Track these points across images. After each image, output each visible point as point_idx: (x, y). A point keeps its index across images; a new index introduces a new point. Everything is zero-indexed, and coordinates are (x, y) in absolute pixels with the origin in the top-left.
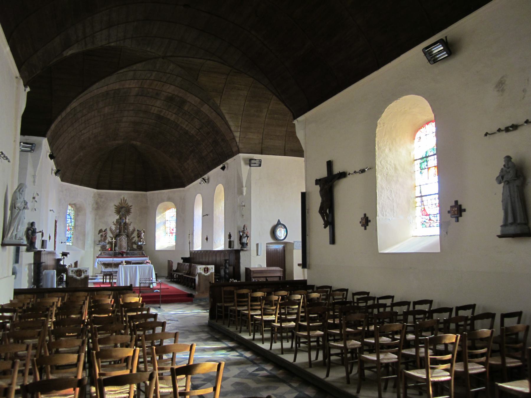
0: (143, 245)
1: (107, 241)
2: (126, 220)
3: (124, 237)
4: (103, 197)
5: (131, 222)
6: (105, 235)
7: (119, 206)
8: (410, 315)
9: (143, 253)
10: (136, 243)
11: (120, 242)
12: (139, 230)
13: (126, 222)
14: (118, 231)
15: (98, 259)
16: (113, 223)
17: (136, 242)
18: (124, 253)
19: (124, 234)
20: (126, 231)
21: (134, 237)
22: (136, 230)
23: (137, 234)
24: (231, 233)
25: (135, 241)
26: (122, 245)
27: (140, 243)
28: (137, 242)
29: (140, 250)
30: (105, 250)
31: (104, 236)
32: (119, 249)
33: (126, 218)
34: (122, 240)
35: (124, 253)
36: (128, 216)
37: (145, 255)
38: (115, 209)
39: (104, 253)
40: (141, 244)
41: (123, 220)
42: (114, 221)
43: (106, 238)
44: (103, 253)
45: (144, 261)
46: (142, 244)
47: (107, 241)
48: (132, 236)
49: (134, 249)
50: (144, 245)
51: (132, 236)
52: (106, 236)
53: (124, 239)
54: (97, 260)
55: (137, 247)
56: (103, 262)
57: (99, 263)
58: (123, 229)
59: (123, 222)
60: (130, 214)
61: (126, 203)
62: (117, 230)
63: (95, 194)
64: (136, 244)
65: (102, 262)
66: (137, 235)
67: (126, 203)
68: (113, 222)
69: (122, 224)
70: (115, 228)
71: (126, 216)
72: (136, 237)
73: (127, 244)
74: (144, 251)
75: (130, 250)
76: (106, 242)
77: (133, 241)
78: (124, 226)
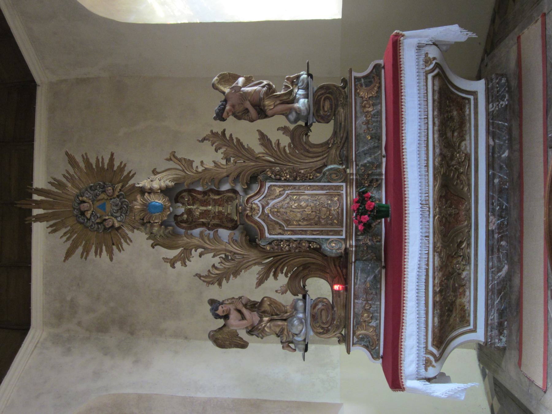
0: (315, 86)
1: (288, 299)
2: (151, 191)
3: (257, 201)
4: (69, 298)
5: (173, 157)
6: (245, 312)
7: (72, 232)
8: (338, 19)
9: (365, 77)
10: (302, 123)
11: (288, 222)
12: (216, 105)
13: (165, 191)
14: (224, 233)
15: (409, 383)
16: (178, 264)
17: (292, 127)
18: (370, 205)
19: (243, 198)
20: (225, 187)
21: (264, 139)
22: (218, 127)
23: (244, 123)
24: (280, 142)
25: (285, 129)
26: (308, 211)
27: (302, 103)
28: (292, 117)
29: (347, 104)
30: (339, 312)
31: (252, 317)
32: (338, 233)
33: (143, 191)
34: (276, 211)
35: (370, 205)
36: (129, 177)
37: (377, 67)
38: (125, 245)
39: (358, 324)
40: (306, 96)
41: (147, 207)
42: (166, 260)
43: (266, 306)
44: (361, 332)
45: (427, 61)
46: (307, 88)
47: (288, 299)
48: (258, 149)
49: (335, 133)
50: (309, 75)
51: (258, 149)
52: (253, 306)
53: (272, 203)
54: (414, 390)
55: (325, 119)
56: (431, 348)
57: (432, 372)
58: (216, 203)
59: (163, 208)
60: (121, 169)
61: (54, 189)
62: (217, 238)
63: (56, 339)
64: (308, 127)
65: (427, 352)
66: (252, 121)
67: (54, 189)
68: (173, 266)
69: (181, 210)
70: (206, 250)
71: (133, 186)
72: (262, 124)
73: (304, 179)
74: (354, 74)
75: (346, 160)
76: (295, 307)
77: (285, 141)
78: (194, 201)
